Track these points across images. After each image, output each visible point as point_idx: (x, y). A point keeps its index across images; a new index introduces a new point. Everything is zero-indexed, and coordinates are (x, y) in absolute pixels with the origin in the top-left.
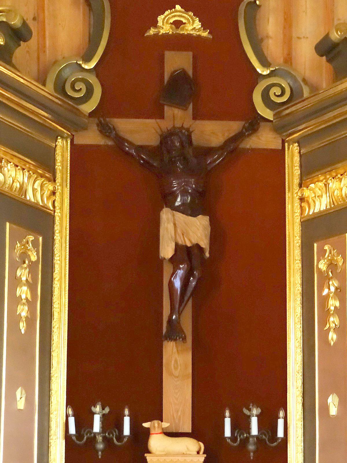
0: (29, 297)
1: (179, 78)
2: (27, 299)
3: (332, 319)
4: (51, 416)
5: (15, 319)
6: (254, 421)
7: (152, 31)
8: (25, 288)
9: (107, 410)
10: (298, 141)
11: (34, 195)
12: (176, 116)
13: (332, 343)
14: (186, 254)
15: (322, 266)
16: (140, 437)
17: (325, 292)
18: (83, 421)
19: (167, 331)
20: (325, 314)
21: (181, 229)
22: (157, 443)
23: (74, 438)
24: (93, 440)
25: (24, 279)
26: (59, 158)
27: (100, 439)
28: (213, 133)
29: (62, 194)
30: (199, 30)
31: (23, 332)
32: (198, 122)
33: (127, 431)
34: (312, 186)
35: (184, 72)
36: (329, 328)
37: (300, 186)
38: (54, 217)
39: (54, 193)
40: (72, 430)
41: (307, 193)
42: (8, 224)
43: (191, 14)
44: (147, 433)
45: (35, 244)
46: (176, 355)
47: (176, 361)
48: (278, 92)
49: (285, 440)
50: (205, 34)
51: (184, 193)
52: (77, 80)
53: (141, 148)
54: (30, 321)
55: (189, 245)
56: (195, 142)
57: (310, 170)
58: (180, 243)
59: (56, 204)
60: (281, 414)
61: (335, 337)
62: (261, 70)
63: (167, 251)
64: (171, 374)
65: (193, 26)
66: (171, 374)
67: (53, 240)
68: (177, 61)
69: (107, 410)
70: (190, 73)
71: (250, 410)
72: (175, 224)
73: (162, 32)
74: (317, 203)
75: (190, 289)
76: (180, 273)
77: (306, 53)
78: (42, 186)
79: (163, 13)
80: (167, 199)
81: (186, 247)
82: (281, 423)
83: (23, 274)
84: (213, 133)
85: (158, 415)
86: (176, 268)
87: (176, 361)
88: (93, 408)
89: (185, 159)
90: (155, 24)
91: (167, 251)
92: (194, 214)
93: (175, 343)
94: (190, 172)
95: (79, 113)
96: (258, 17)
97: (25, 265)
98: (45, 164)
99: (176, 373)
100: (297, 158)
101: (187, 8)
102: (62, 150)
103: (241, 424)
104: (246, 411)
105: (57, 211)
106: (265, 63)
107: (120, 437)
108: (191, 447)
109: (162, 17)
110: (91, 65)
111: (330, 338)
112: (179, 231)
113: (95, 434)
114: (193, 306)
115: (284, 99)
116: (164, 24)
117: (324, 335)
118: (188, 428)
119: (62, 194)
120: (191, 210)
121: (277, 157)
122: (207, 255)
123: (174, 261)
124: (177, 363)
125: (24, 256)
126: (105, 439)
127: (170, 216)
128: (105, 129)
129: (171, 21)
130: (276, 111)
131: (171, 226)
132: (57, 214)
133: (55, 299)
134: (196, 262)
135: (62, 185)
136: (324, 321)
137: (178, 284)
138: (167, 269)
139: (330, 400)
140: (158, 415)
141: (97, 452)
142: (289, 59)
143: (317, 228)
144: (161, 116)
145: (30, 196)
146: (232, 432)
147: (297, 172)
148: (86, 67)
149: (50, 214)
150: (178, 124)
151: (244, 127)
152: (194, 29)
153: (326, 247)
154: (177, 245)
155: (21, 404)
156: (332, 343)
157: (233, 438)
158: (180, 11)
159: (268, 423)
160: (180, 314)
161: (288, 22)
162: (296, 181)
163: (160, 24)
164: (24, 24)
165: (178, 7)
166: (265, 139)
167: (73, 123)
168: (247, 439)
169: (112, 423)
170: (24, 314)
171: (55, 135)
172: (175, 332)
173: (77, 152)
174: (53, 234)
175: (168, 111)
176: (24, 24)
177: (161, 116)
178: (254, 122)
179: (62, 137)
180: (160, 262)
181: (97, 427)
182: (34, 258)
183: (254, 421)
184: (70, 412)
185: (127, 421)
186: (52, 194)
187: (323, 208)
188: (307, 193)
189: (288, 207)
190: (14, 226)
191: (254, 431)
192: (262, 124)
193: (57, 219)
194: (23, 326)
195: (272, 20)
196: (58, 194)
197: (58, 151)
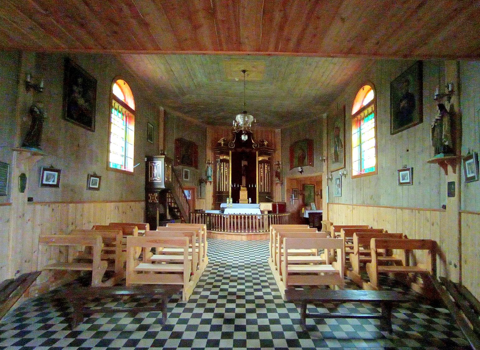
12: (243, 148)
16: (240, 187)
18: (233, 186)
22: (242, 188)
63: (243, 165)
85: (241, 185)
91: (243, 165)
102: (230, 152)
103: (251, 186)
117: (261, 174)
120: (246, 160)
140: (241, 185)
143: (260, 162)
159: (254, 186)
166: (254, 151)
169: (236, 186)
186: (229, 158)
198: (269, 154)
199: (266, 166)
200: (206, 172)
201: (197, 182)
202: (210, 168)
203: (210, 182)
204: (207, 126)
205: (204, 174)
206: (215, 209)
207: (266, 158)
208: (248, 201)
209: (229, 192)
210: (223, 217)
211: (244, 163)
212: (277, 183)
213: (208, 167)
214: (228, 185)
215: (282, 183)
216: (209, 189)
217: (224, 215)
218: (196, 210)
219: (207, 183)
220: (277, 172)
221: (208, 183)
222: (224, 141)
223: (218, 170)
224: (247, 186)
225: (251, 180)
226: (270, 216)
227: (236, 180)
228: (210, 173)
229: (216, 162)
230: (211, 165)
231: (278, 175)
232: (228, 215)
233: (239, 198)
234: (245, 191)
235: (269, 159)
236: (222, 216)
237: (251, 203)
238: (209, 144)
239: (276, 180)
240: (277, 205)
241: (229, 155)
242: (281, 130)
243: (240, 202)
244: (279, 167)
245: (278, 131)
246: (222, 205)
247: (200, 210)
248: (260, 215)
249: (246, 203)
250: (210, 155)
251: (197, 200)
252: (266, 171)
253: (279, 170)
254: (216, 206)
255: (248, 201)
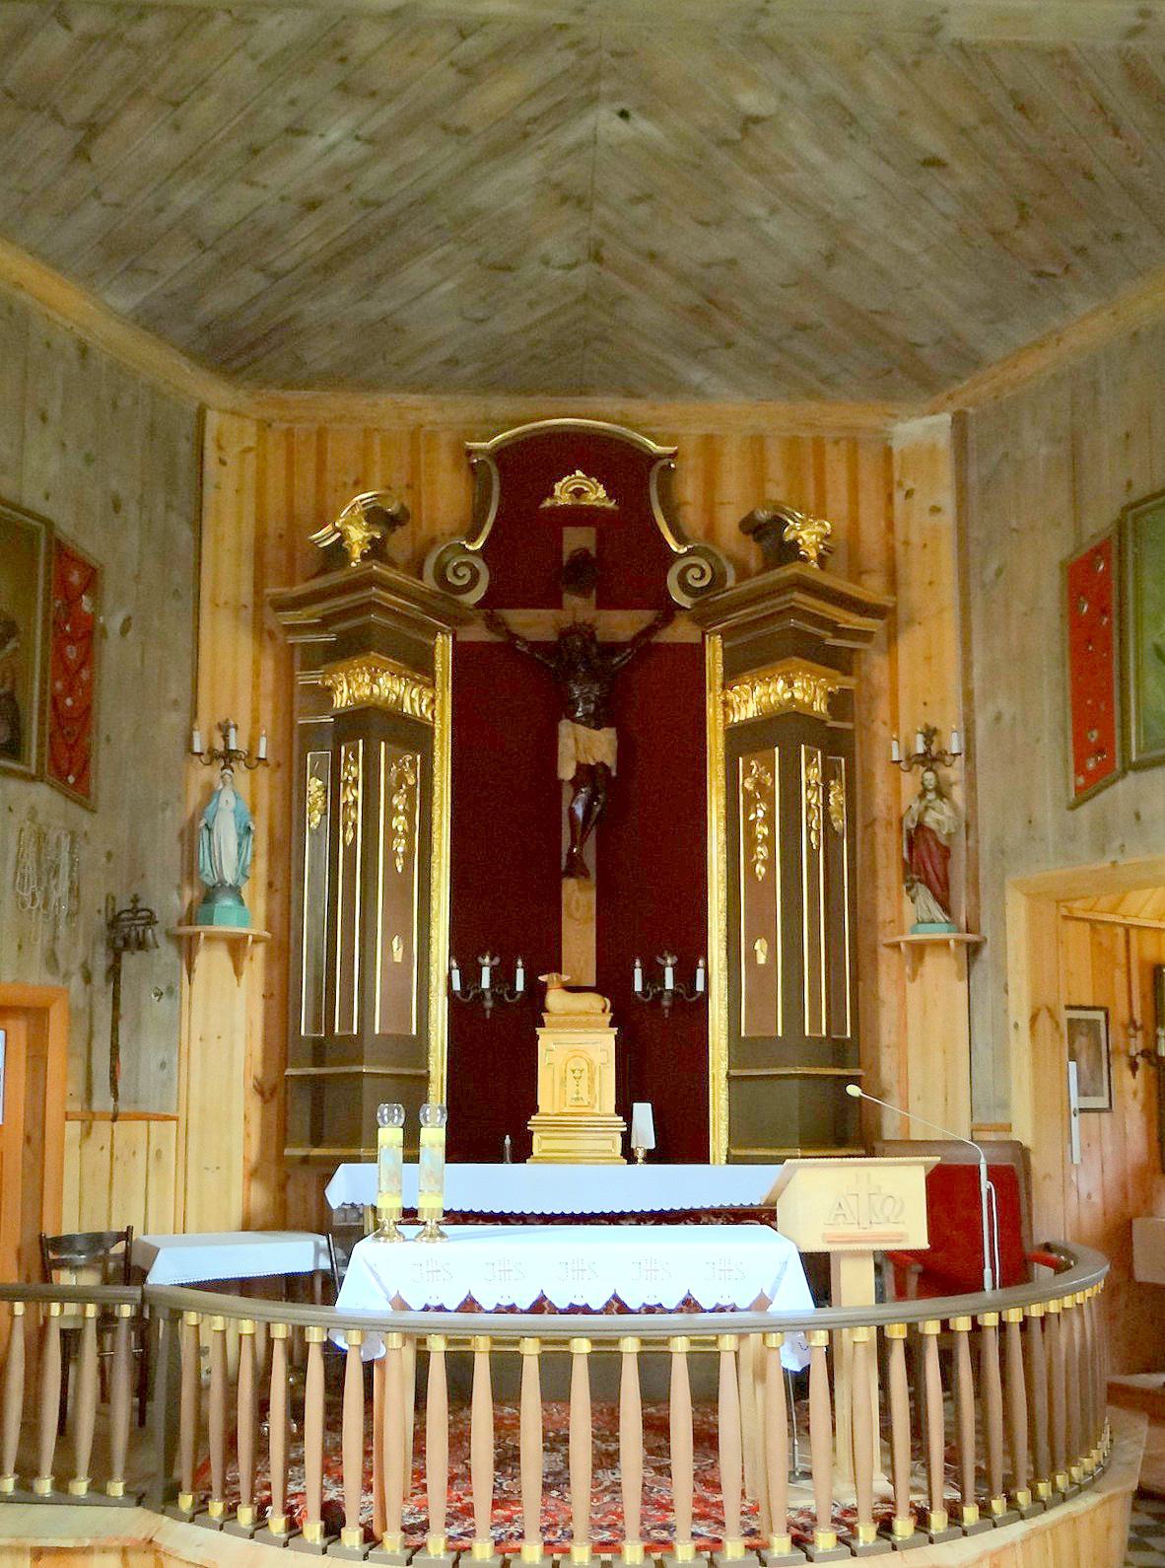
0: (406, 827)
1: (581, 559)
2: (404, 831)
3: (759, 849)
4: (432, 968)
5: (391, 855)
6: (669, 972)
7: (548, 503)
8: (402, 818)
9: (497, 961)
10: (723, 633)
11: (412, 706)
12: (578, 607)
13: (760, 878)
14: (588, 774)
15: (749, 785)
16: (536, 994)
17: (752, 817)
18: (470, 975)
19: (568, 866)
20: (752, 842)
21: (584, 745)
22: (555, 999)
23: (458, 995)
24: (480, 996)
25: (401, 807)
26: (438, 658)
27: (488, 995)
28: (622, 625)
29: (442, 701)
30: (603, 500)
31: (400, 870)
32: (604, 612)
33: (520, 986)
34: (737, 688)
35: (586, 551)
36: (757, 860)
37: (724, 686)
38: (433, 729)
39: (433, 701)
40: (457, 986)
41: (731, 695)
42: (383, 744)
43: (594, 480)
44: (544, 987)
45: (413, 764)
46: (577, 894)
47: (577, 902)
48: (696, 573)
49: (706, 994)
50: (611, 505)
51: (587, 701)
52: (459, 565)
53: (535, 646)
54: (408, 856)
55: (592, 763)
56: (599, 639)
57: (734, 672)
58: (582, 761)
59: (436, 714)
60: (701, 963)
61: (763, 870)
62: (674, 547)
63: (567, 771)
64: (570, 916)
65: (597, 495)
66: (570, 916)
67: (433, 756)
68: (577, 540)
69: (497, 961)
70: (593, 552)
71: (665, 959)
72: (576, 740)
73: (561, 503)
74: (743, 709)
75: (594, 817)
76: (582, 796)
77: (729, 519)
78: (420, 694)
79: (560, 480)
80: (566, 709)
81: (589, 765)
82: (700, 973)
83: (399, 801)
84: (622, 625)
85: (556, 967)
86: (577, 791)
87: (577, 902)
88: (480, 960)
89: (587, 662)
90: (551, 493)
91: (567, 771)
92: (598, 727)
93: (1155, 1286)
94: (594, 676)
95: (459, 605)
96: (673, 483)
97: (402, 791)
98: (419, 666)
99: (577, 915)
100: (720, 654)
101: (589, 473)
102: (443, 648)
103: (653, 976)
104: (660, 960)
105: (438, 722)
106: (681, 540)
107: (512, 993)
108: (595, 1003)
109: (561, 484)
110: (479, 545)
111: (757, 871)
112: (581, 746)
113: (483, 991)
114: (597, 837)
115: (705, 582)
116: (562, 493)
117: (751, 869)
118: (592, 982)
119: (442, 701)
120: (596, 721)
121: (697, 652)
122: (614, 774)
123: (576, 783)
124: (579, 902)
125: (401, 779)
126: (494, 995)
127: (570, 729)
128: (493, 623)
129: (571, 489)
130: (696, 600)
131: (571, 742)
132: (438, 725)
133: (723, 963)
134: (601, 783)
135: (442, 691)
136: (750, 853)
137: (579, 811)
138: (567, 793)
139: (757, 946)
140: (556, 967)
141: (485, 1010)
142: (710, 531)
143: (746, 739)
144: (557, 604)
145: (407, 709)
146: (644, 986)
147: (720, 670)
148: (471, 548)
149: (427, 727)
150: (580, 620)
151: (656, 619)
152: (597, 499)
153: (753, 763)
154: (578, 762)
155: (398, 956)
156: (760, 878)
157: (645, 993)
158: (580, 478)
159: (686, 975)
160: (582, 844)
161: (710, 483)
162: (719, 681)
163: (557, 493)
164: (403, 508)
165: (579, 473)
166: (681, 632)
167: (455, 619)
168: (661, 993)
169: (503, 976)
170: (400, 849)
171: (433, 632)
172: (576, 868)
173: (460, 650)
174: (433, 751)
175: (571, 600)
176: (403, 508)
177: (557, 604)
178: (669, 611)
179: (443, 633)
180: (559, 783)
181: (486, 983)
182: (411, 781)
183: (669, 972)
184: (454, 964)
185: (520, 974)
186: (431, 704)
187: (750, 715)
188: (731, 695)
189: (710, 711)
190: (391, 746)
191: (669, 984)
192: (677, 613)
193: (437, 731)
194: (399, 864)
195: (690, 481)
196: (437, 701)
197: (438, 650)
198: (836, 660)
199: (810, 774)
200: (191, 837)
201: (84, 947)
202: (227, 801)
203: (236, 946)
204: (217, 394)
205: (166, 852)
206: (280, 1220)
207: (802, 689)
208: (626, 1137)
209: (418, 1047)
210: (328, 1346)
211: (584, 745)
212: (919, 950)
213: (210, 793)
214: (416, 973)
215: (973, 950)
216: (218, 1028)
217: (347, 1325)
218: (60, 1243)
219: (201, 960)
220: (918, 837)
221: (212, 961)
222: (374, 515)
223: (315, 819)
224: (610, 982)
225: (655, 915)
226: (932, 1328)
227: (502, 914)
228: (229, 850)
229: (297, 742)
230: (241, 775)
231: (928, 862)
232: (382, 1327)
233: (530, 1105)
234: (589, 1025)
235: (839, 703)
236: (315, 1336)
237: (652, 1157)
238: (227, 571)
239: (909, 914)
240: (985, 1184)
241: (432, 673)
242: (960, 421)
243: (538, 1144)
244: (941, 793)
245: (920, 430)
246: (344, 1188)
247: (97, 1241)
248: (806, 1328)
249: (610, 1160)
250: (234, 676)
251: (73, 1129)
252: (810, 838)
253: (940, 817)
254: (293, 1194)
255: (626, 1137)
